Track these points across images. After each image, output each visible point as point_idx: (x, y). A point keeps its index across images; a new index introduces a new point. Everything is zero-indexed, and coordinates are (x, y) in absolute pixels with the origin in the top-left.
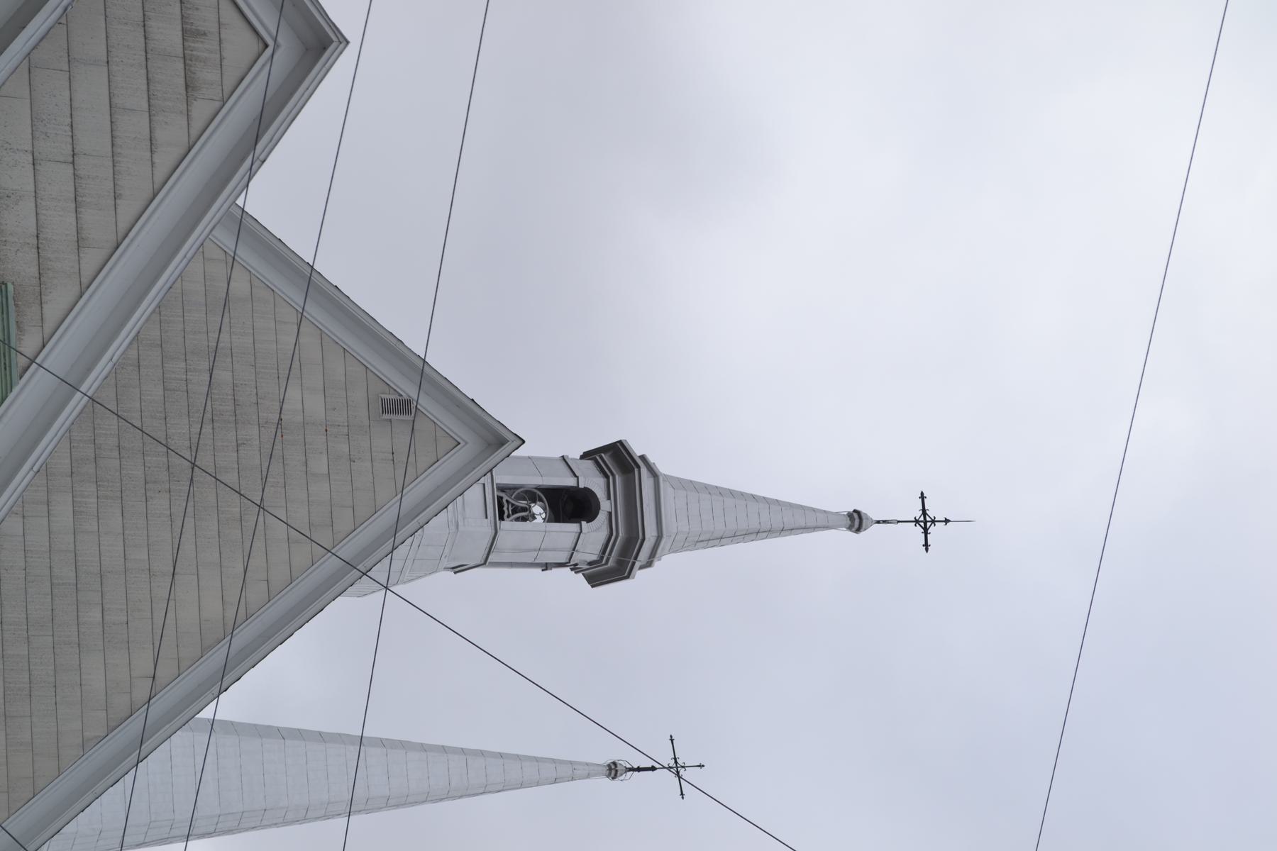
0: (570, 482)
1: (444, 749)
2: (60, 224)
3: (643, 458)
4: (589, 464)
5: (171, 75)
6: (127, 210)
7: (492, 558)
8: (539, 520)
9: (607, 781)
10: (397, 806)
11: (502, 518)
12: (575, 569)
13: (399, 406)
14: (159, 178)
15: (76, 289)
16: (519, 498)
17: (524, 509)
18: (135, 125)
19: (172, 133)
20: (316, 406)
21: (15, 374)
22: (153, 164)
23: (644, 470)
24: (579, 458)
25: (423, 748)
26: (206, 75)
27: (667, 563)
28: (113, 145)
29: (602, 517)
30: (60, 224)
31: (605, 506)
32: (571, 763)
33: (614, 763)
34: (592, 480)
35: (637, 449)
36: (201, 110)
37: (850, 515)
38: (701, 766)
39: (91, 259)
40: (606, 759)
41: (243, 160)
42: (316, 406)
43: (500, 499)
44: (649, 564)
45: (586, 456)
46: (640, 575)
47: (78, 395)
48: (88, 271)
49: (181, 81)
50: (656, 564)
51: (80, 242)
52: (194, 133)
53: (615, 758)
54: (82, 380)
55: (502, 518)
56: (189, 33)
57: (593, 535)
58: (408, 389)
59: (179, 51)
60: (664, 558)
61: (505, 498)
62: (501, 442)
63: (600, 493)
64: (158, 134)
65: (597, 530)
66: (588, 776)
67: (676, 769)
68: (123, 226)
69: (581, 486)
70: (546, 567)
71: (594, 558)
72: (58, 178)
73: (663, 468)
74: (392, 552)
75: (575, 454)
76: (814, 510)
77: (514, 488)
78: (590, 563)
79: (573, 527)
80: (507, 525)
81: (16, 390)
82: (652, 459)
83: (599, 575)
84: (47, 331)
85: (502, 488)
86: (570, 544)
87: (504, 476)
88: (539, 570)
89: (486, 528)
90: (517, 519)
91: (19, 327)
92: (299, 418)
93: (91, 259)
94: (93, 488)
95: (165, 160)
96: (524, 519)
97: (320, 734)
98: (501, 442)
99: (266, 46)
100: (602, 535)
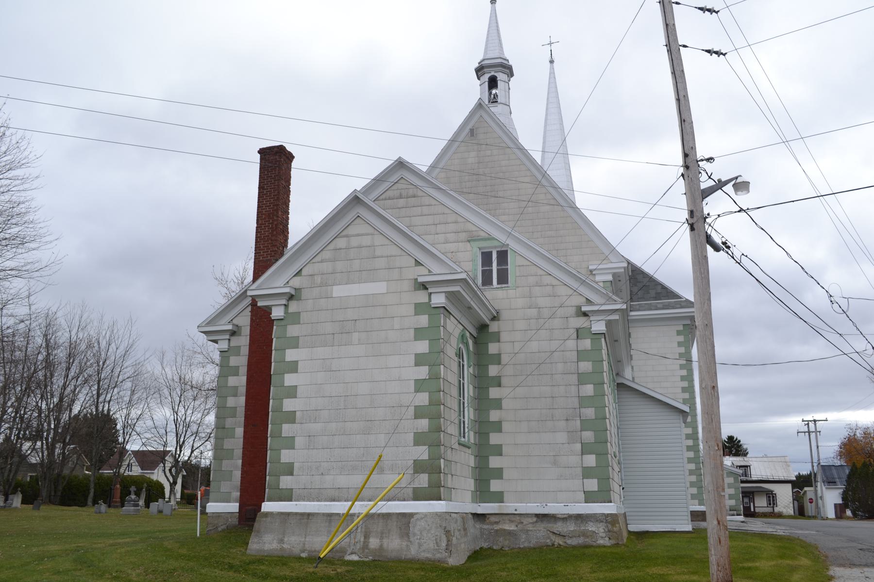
0: (487, 84)
1: (547, 109)
2: (452, 227)
3: (479, 63)
4: (481, 78)
5: (412, 201)
6: (447, 211)
7: (508, 104)
8: (497, 91)
9: (554, 63)
10: (562, 122)
11: (497, 102)
12: (509, 81)
13: (472, 132)
14: (438, 203)
15: (468, 223)
16: (491, 97)
17: (494, 96)
18: (426, 210)
19: (427, 200)
20: (473, 154)
21: (491, 237)
22: (435, 205)
23: (483, 63)
24: (479, 81)
25: (547, 115)
26: (411, 192)
27: (507, 55)
28: (431, 215)
29: (496, 74)
30: (452, 227)
31: (493, 73)
32: (550, 73)
33: (550, 61)
34: (486, 78)
35: (477, 65)
36: (420, 193)
37: (492, 3)
38: (550, 37)
39: (460, 219)
40: (549, 64)
41: (448, 193)
42: (473, 154)
43: (492, 102)
44: (508, 60)
45: (479, 79)
46: (511, 63)
47: (512, 232)
48: (463, 220)
49: (413, 199)
50: (508, 58)
51: (456, 222)
52: (426, 195)
53: (548, 62)
54: (508, 232)
55: (497, 102)
56: (401, 197)
57: (501, 76)
58: (467, 130)
59: (406, 199)
60: (506, 56)
61: (491, 101)
62: (480, 104)
63: (489, 75)
64: (427, 204)
65: (499, 75)
66: (553, 69)
67: (550, 44)
68: (451, 212)
69: (488, 80)
70: (509, 89)
71: (507, 76)
72: (440, 228)
73: (481, 58)
74: (845, 354)
75: (479, 82)
76: (491, 14)
77: (489, 98)
78: (508, 77)
79: (499, 82)
80: (499, 101)
81: (495, 237)
82: (479, 61)
83: (511, 74)
84: (479, 229)
85: (489, 102)
86: (504, 82)
87: (487, 102)
88: (510, 91)
89: (500, 106)
90: (497, 97)
91: (479, 236)
92: (477, 158)
93: (460, 219)
94: (497, 211)
95: (434, 202)
96: (497, 96)
97: (543, 143)
98: (480, 104)
99: (402, 177)
100: (501, 74)
